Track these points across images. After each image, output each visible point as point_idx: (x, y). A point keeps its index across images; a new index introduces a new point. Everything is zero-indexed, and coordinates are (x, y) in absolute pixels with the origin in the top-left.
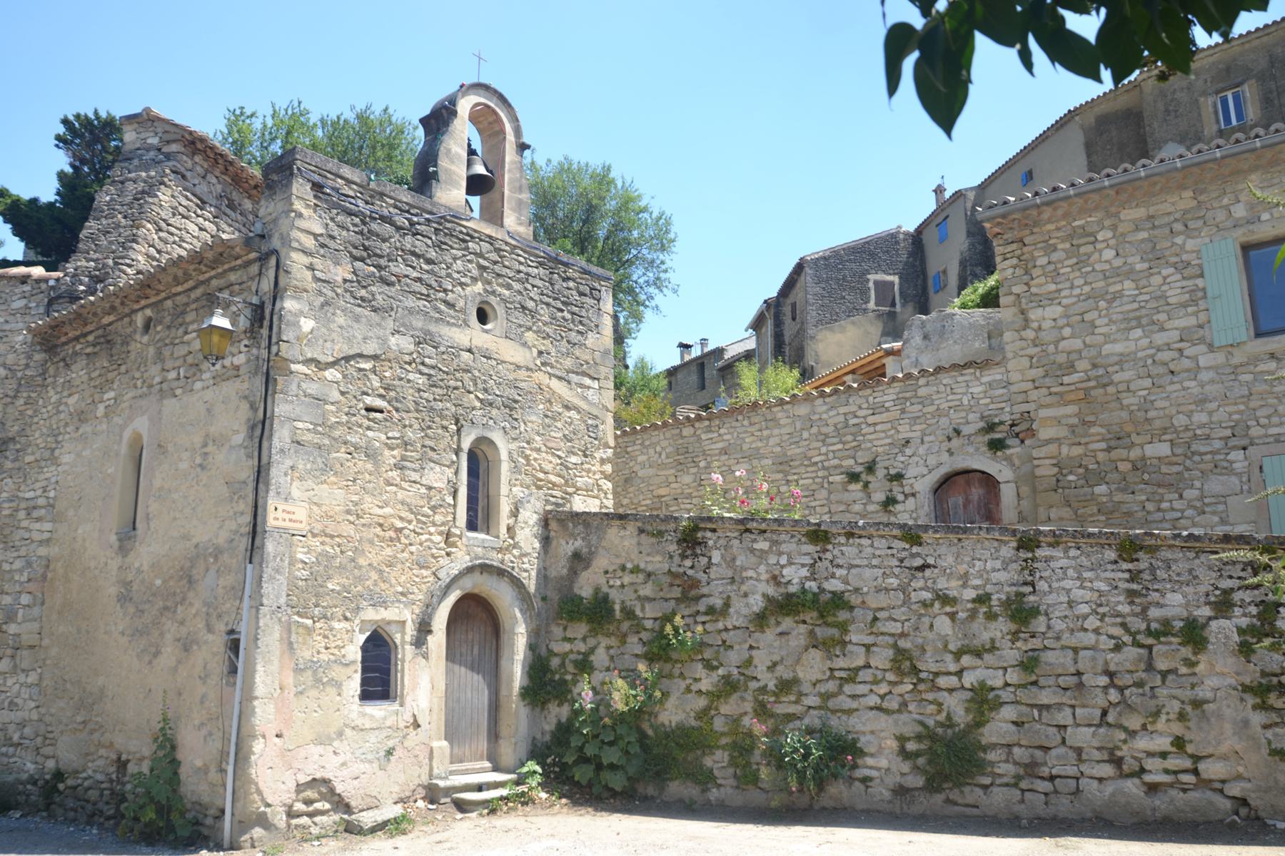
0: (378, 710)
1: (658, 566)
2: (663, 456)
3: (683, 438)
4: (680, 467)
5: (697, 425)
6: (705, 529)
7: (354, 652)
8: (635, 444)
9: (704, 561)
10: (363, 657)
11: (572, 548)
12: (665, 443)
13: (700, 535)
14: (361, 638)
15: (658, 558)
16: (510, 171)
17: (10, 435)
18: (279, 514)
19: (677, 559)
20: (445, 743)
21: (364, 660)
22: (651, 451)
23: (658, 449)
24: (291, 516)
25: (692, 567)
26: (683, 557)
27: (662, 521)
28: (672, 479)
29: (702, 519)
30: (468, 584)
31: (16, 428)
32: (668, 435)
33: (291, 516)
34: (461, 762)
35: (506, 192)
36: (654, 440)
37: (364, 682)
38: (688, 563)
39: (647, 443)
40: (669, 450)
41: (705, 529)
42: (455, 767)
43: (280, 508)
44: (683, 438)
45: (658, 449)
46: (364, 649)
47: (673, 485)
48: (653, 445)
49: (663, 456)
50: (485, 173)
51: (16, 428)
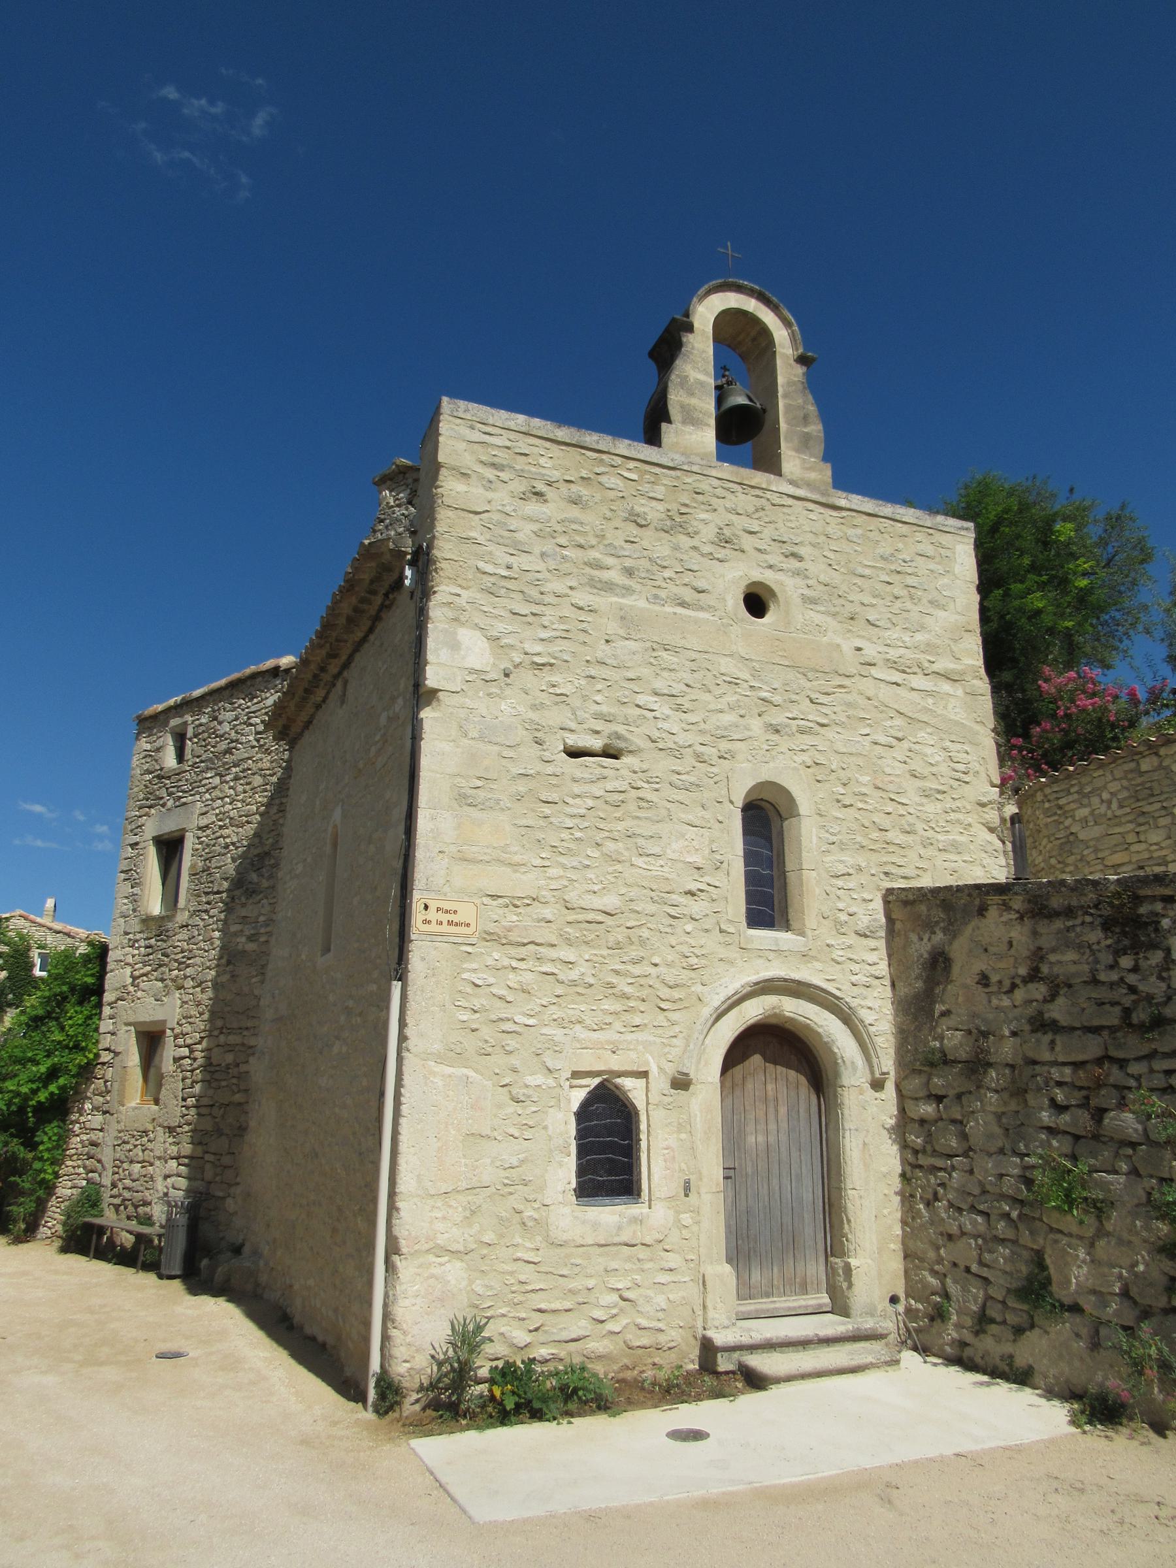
0: (609, 1215)
1: (1073, 969)
2: (1115, 805)
3: (1141, 774)
4: (1141, 820)
5: (1162, 751)
6: (1154, 898)
7: (564, 1127)
8: (1069, 793)
9: (1157, 957)
10: (578, 1131)
11: (929, 947)
12: (1114, 787)
13: (1143, 910)
14: (578, 1096)
15: (1071, 956)
16: (785, 396)
17: (266, 849)
18: (432, 915)
19: (1106, 958)
20: (728, 1268)
21: (581, 1135)
22: (1095, 800)
23: (1105, 796)
24: (451, 917)
25: (1135, 969)
26: (1118, 953)
27: (1073, 890)
28: (1131, 838)
29: (1145, 881)
30: (754, 1011)
31: (271, 840)
32: (1118, 773)
33: (451, 917)
34: (767, 1295)
35: (783, 426)
36: (1098, 783)
37: (581, 1171)
38: (1126, 962)
39: (1088, 789)
40: (1124, 794)
41: (1154, 898)
42: (750, 1306)
43: (433, 906)
44: (1141, 774)
45: (1105, 796)
46: (583, 1114)
47: (1134, 848)
48: (1096, 791)
49: (1115, 805)
50: (747, 402)
51: (271, 840)
